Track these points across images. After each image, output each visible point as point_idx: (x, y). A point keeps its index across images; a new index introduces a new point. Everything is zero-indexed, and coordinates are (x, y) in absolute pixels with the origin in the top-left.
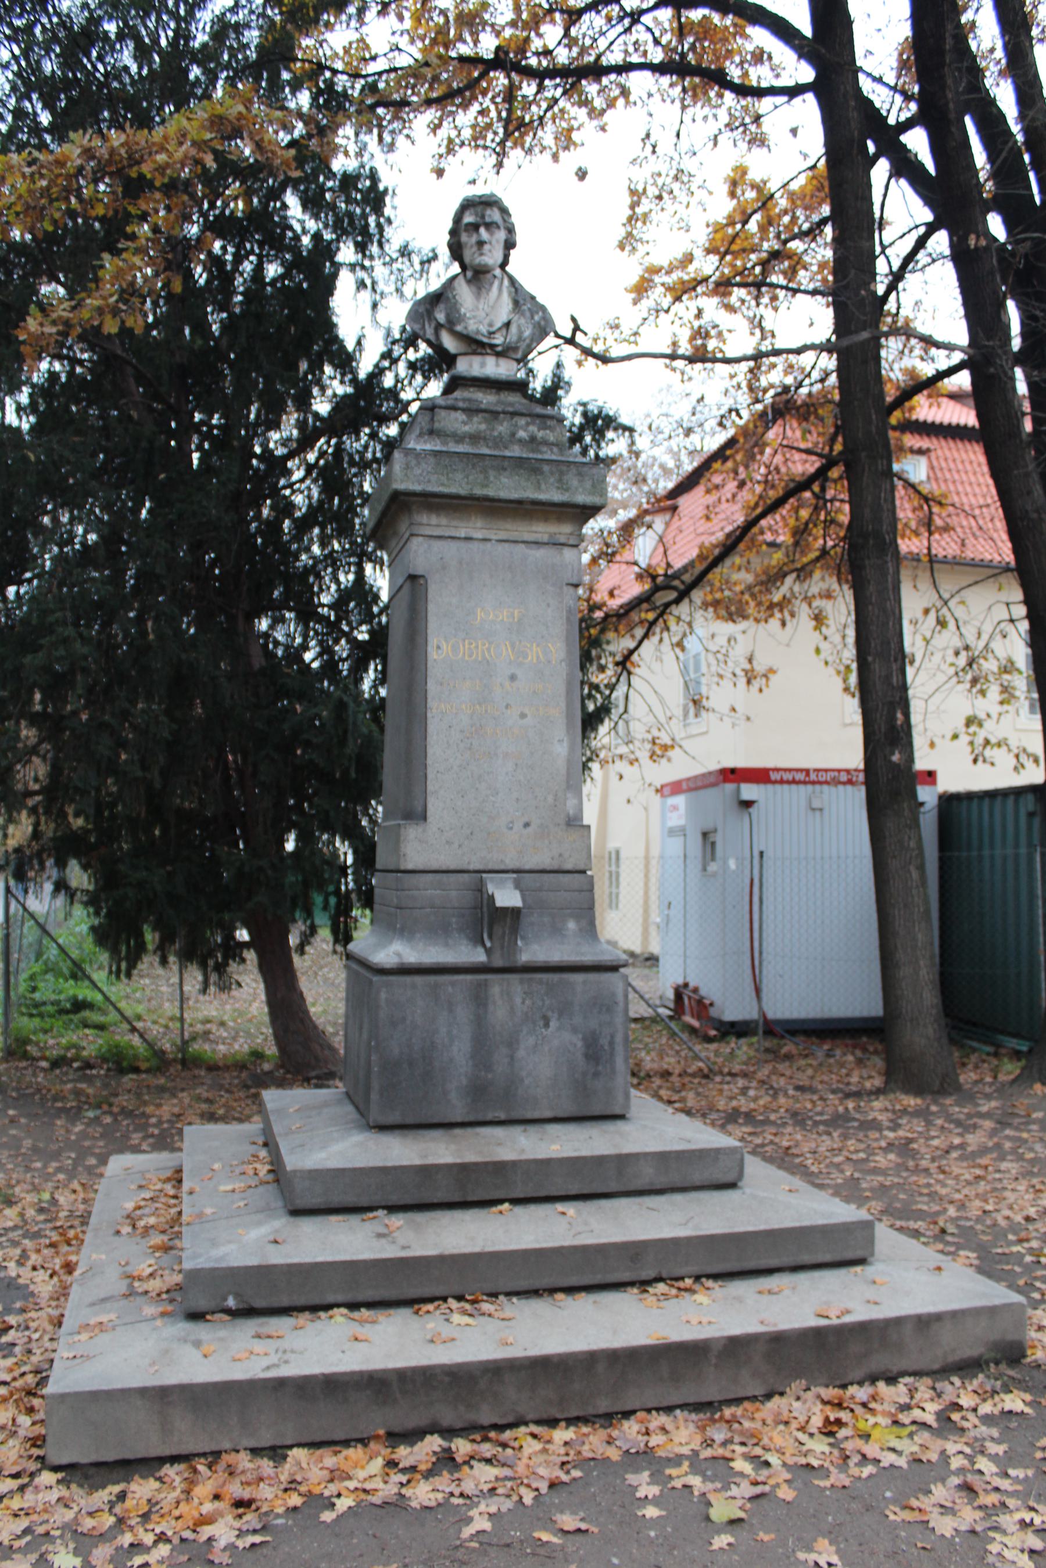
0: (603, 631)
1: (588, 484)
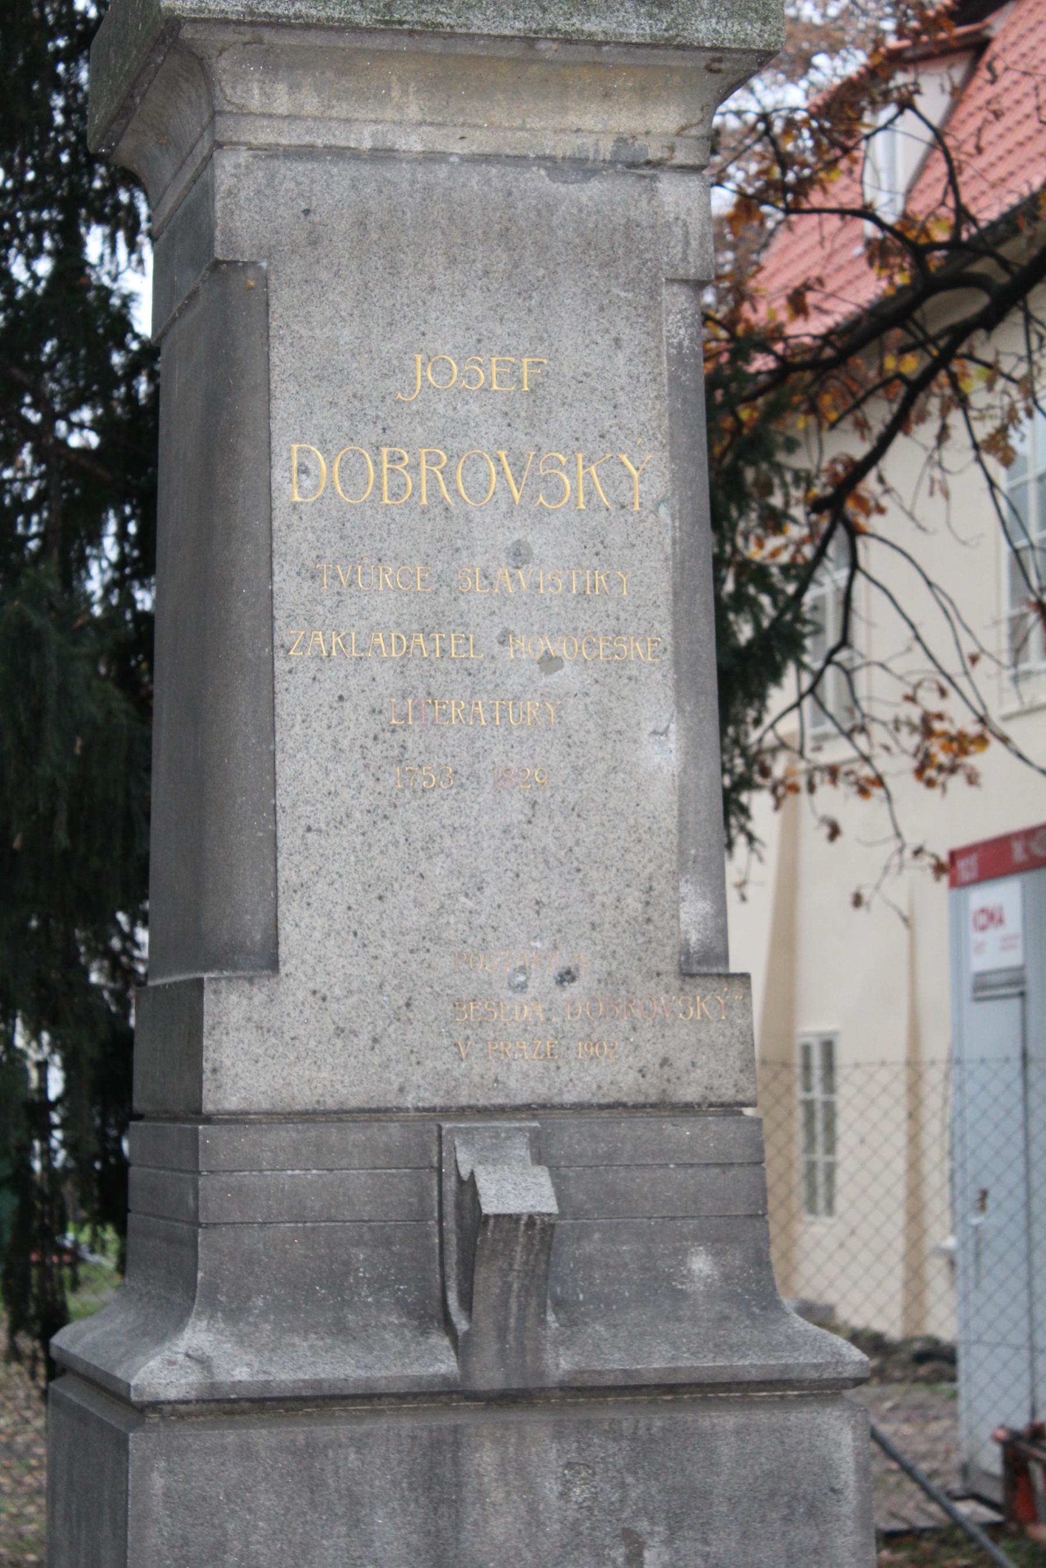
0: (774, 412)
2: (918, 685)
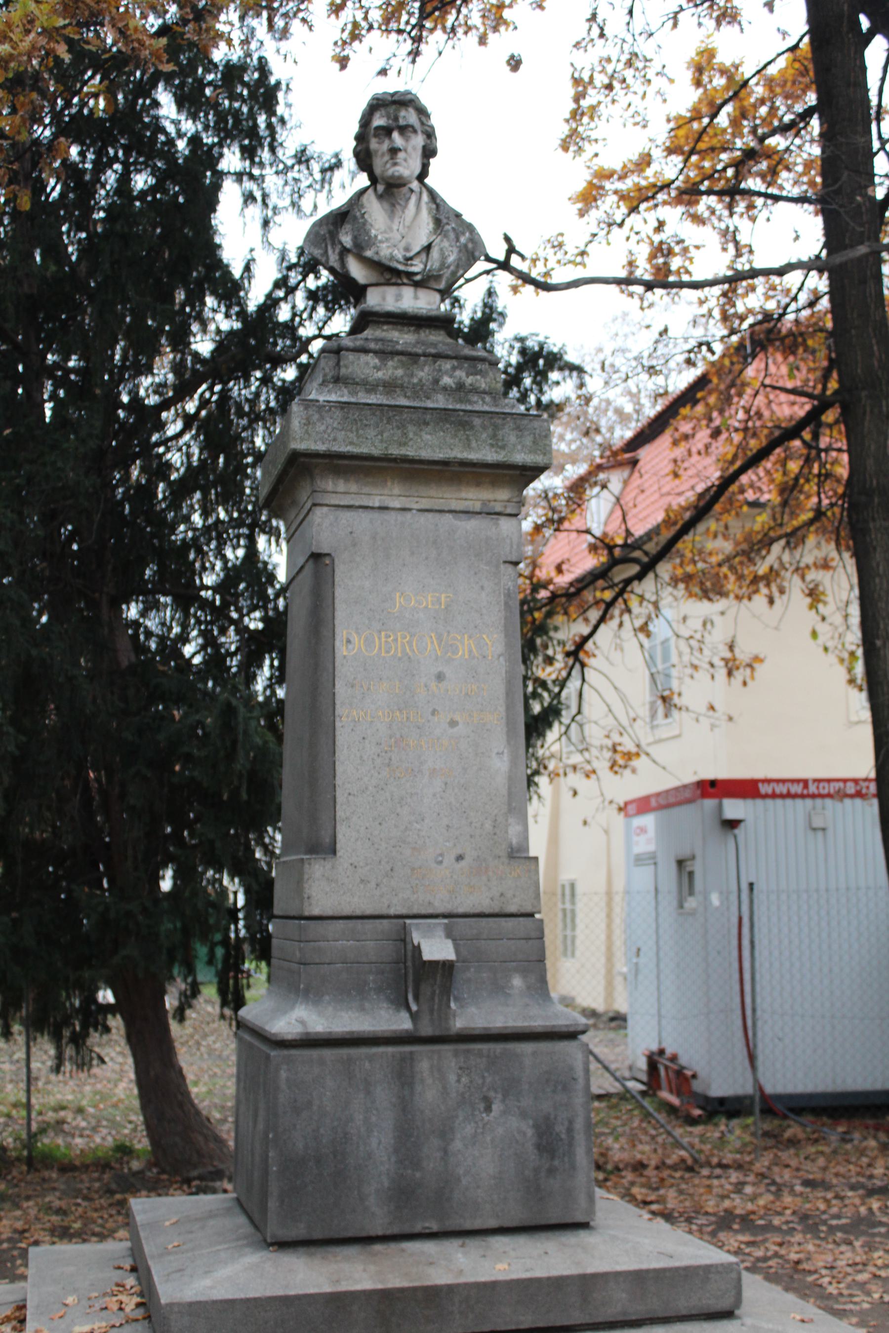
0: (550, 615)
1: (528, 441)
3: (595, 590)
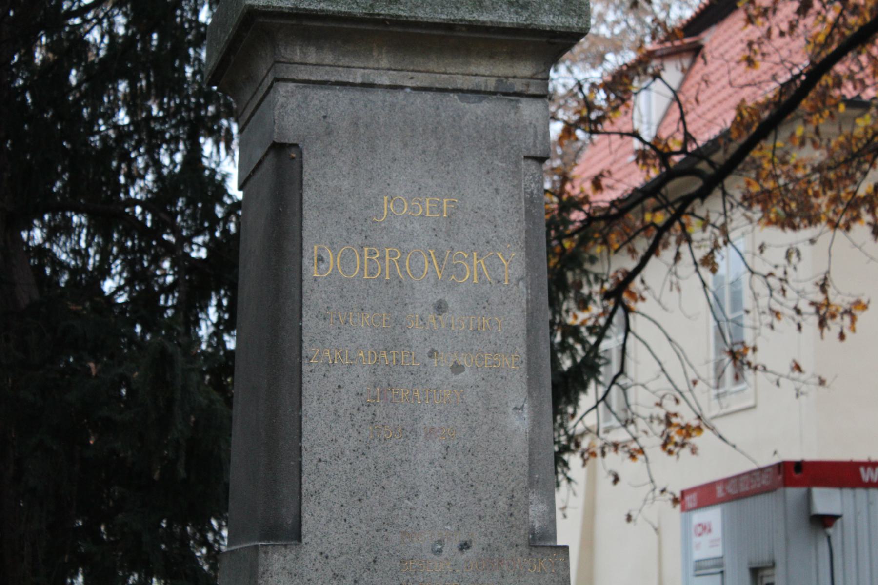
0: (584, 241)
2: (663, 397)
3: (644, 211)
